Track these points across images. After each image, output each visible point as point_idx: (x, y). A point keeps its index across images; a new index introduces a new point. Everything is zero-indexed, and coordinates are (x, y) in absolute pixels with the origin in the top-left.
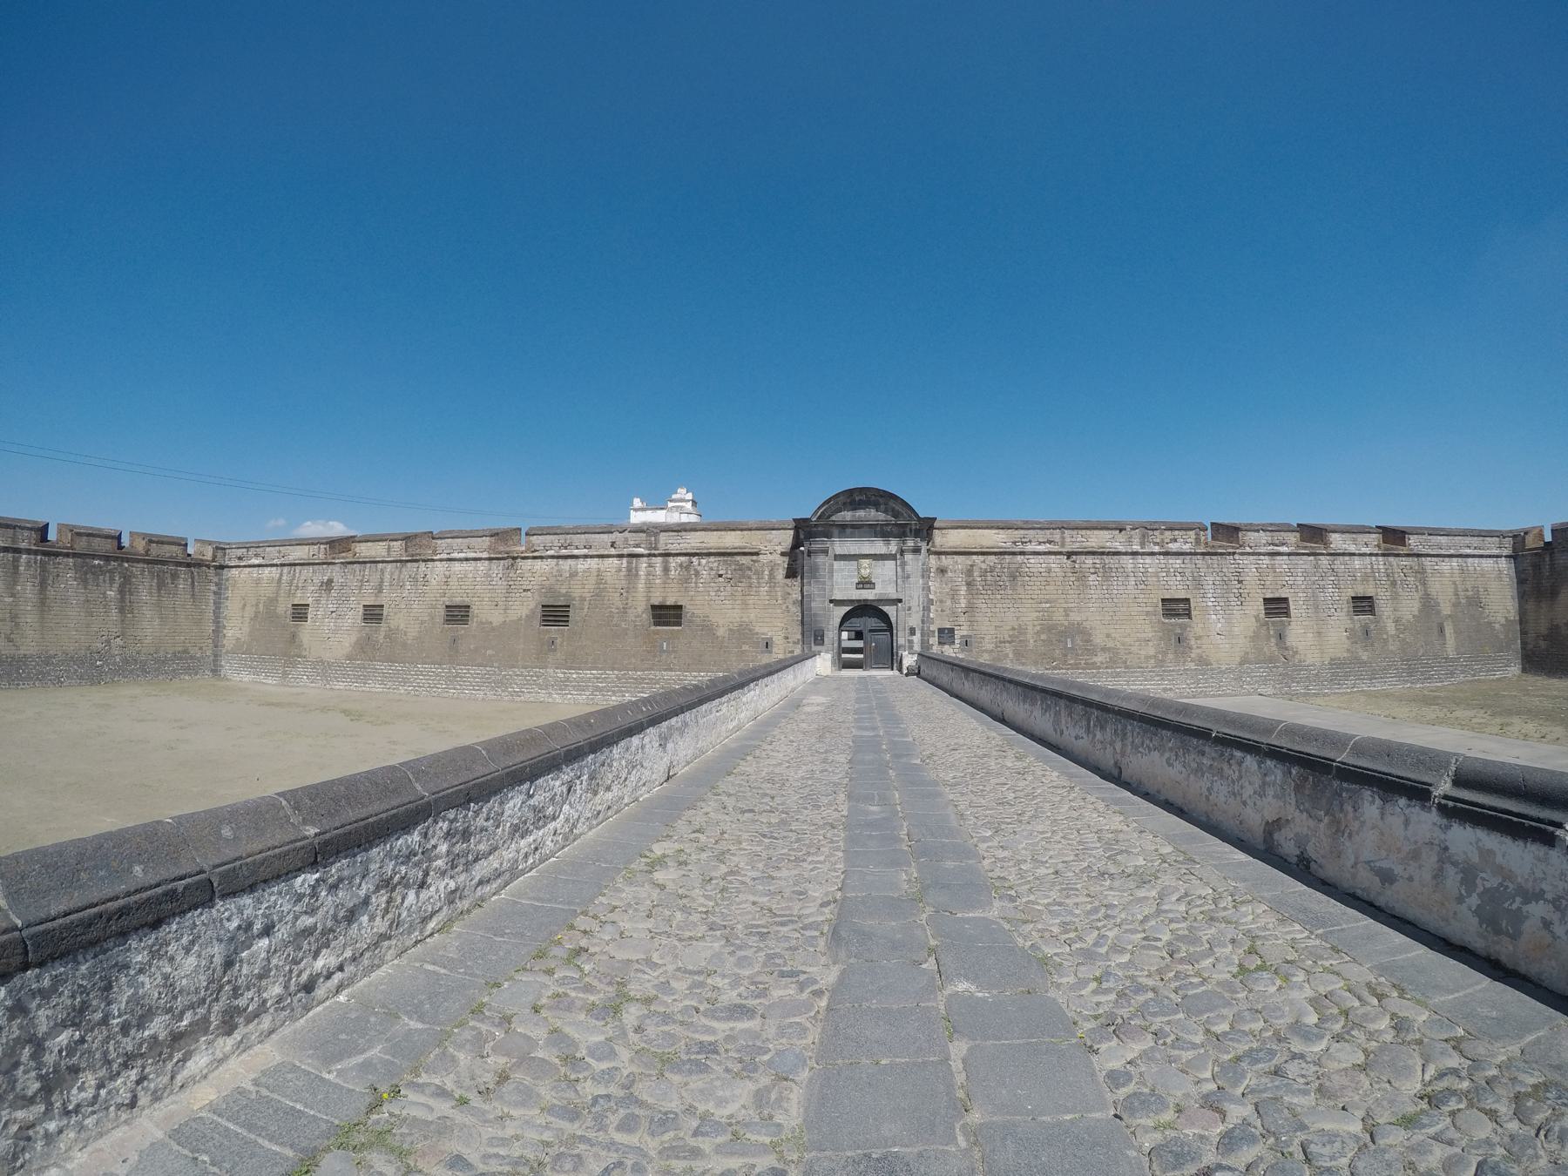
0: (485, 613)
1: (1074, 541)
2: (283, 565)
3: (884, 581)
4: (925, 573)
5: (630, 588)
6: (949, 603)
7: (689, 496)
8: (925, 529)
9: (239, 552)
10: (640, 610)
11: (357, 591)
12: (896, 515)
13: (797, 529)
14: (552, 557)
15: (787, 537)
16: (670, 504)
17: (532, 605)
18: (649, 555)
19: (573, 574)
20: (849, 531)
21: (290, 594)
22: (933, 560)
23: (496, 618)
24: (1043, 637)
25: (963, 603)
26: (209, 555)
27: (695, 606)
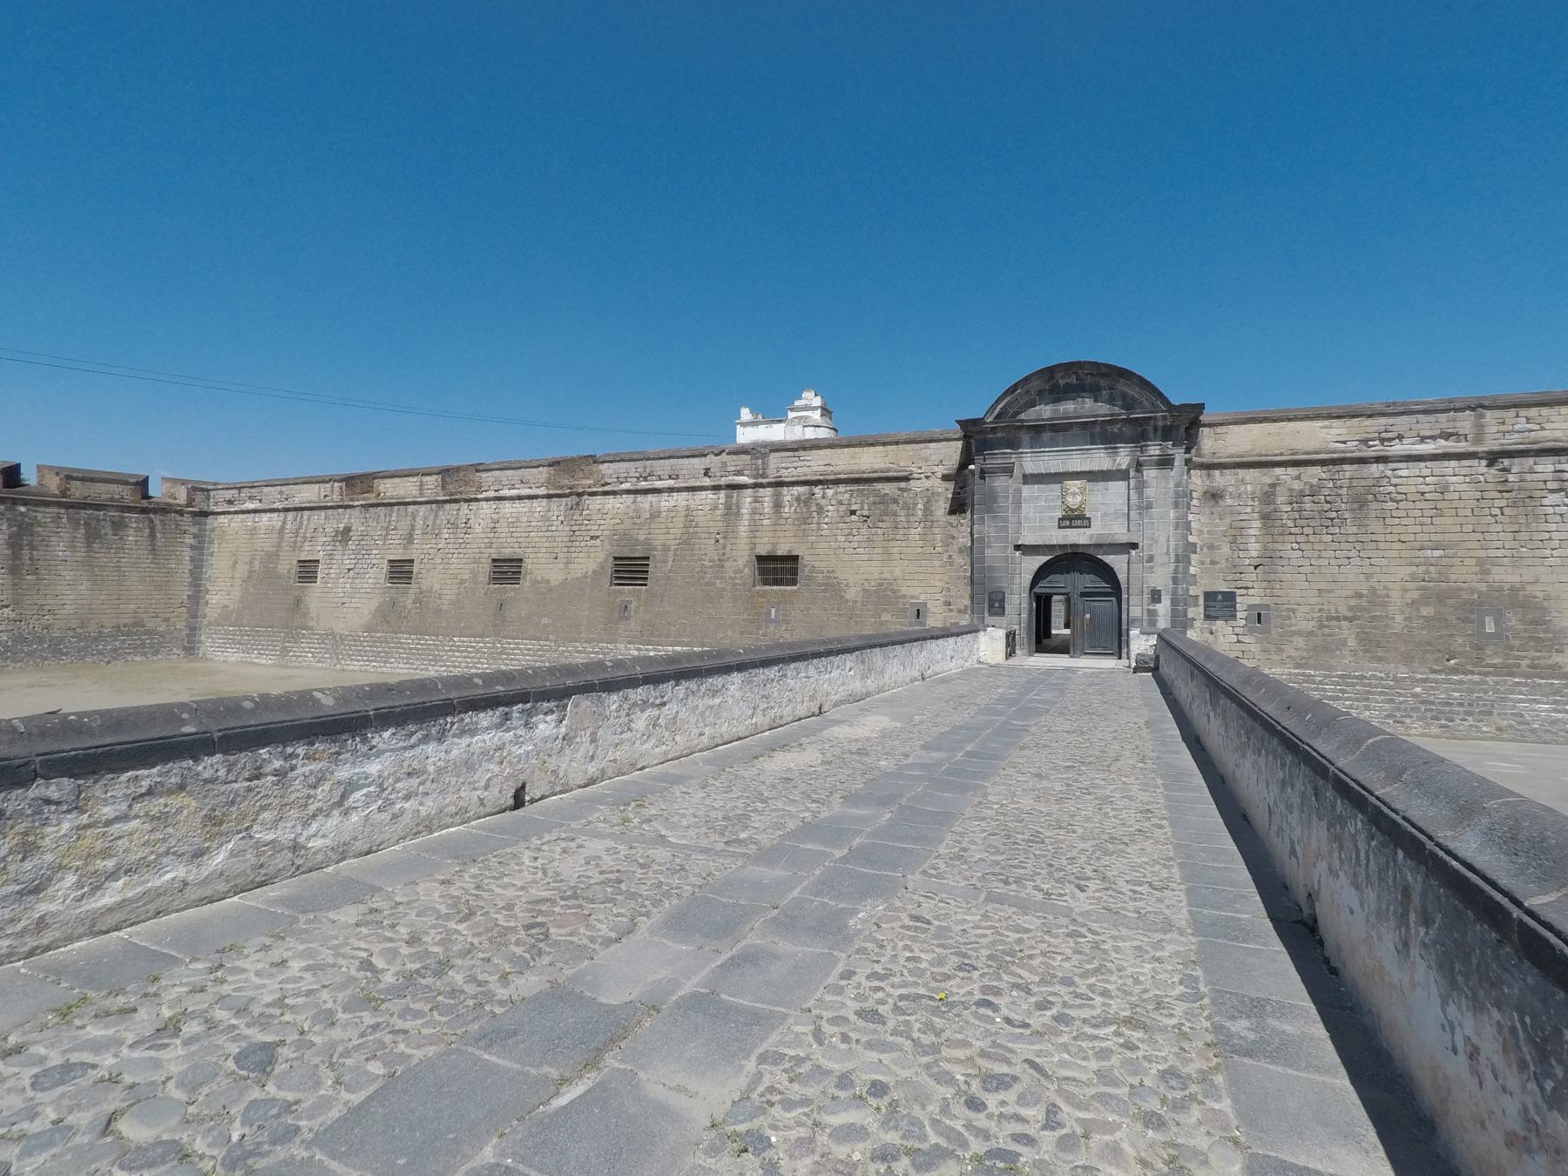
0: (541, 568)
1: (1500, 430)
2: (286, 510)
3: (1107, 513)
4: (1182, 499)
5: (728, 533)
6: (1225, 549)
7: (817, 402)
8: (1184, 425)
9: (229, 494)
10: (741, 562)
11: (381, 540)
12: (1129, 405)
13: (966, 438)
14: (628, 492)
15: (951, 453)
16: (791, 415)
17: (601, 556)
18: (756, 486)
19: (655, 515)
20: (1047, 436)
21: (295, 547)
22: (1198, 480)
23: (555, 574)
24: (1426, 611)
25: (1254, 549)
26: (182, 498)
27: (817, 555)
